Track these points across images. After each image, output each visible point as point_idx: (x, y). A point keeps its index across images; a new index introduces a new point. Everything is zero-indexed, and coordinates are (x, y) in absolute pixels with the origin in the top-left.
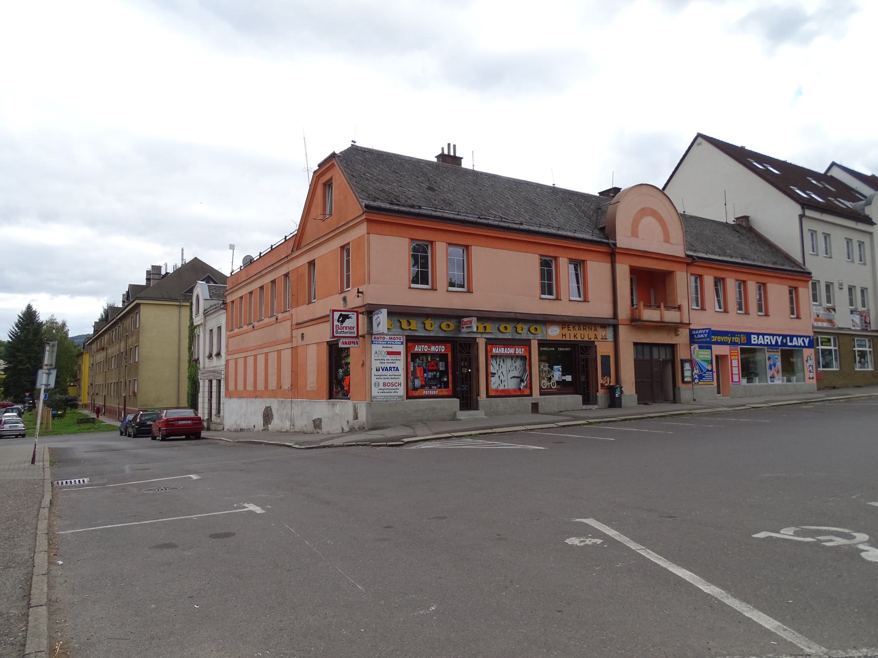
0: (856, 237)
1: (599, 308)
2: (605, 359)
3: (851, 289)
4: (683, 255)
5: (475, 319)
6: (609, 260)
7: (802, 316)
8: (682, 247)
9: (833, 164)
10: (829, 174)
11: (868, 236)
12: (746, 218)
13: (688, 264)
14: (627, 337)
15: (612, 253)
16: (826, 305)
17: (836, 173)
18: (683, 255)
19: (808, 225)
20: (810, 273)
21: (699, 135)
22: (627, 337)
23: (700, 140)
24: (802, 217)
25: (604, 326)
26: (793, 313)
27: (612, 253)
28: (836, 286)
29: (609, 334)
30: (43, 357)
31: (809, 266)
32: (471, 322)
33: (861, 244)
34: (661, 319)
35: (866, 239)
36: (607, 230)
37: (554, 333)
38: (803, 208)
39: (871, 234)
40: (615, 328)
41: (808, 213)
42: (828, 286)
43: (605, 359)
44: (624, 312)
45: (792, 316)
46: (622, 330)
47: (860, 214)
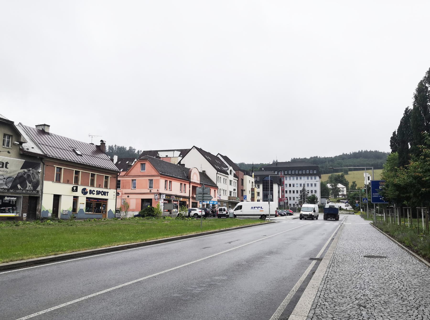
0: (225, 178)
1: (187, 195)
2: (188, 205)
3: (224, 190)
4: (199, 183)
5: (174, 197)
6: (189, 184)
7: (186, 192)
8: (199, 181)
9: (219, 154)
10: (217, 156)
11: (227, 178)
12: (205, 171)
13: (200, 185)
14: (191, 200)
15: (190, 183)
16: (219, 194)
17: (219, 156)
18: (199, 183)
19: (218, 175)
20: (218, 187)
21: (194, 146)
22: (191, 200)
23: (194, 148)
24: (217, 173)
25: (188, 198)
26: (180, 191)
27: (190, 183)
28: (221, 190)
29: (188, 200)
30: (77, 202)
31: (218, 185)
32: (174, 197)
33: (226, 179)
34: (269, 203)
35: (227, 178)
36: (188, 177)
37: (181, 199)
38: (217, 172)
39: (228, 177)
40: (189, 199)
41: (219, 173)
42: (220, 189)
43: (188, 205)
44: (191, 195)
45: (165, 189)
46: (191, 199)
47: (226, 171)
